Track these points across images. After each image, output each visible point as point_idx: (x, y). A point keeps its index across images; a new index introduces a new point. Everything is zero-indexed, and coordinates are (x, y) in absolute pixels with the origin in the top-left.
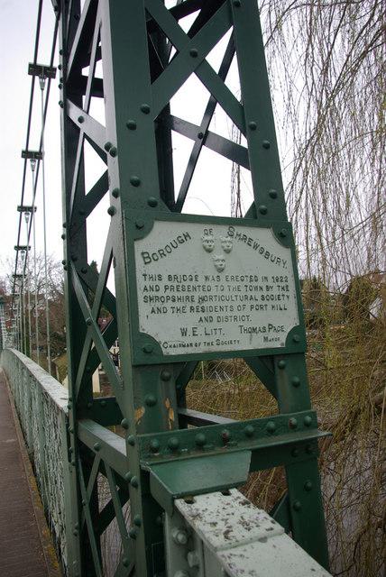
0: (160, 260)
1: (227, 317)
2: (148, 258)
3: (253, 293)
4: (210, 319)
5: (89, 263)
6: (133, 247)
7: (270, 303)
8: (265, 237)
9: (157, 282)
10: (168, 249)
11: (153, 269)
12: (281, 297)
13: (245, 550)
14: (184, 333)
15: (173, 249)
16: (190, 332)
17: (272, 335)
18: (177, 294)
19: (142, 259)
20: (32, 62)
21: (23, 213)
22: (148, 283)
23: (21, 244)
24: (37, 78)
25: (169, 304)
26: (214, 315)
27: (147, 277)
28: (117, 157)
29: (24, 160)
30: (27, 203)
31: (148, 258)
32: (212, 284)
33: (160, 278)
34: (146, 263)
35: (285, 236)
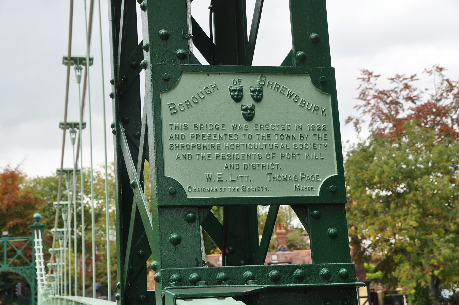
0: (174, 150)
1: (254, 165)
2: (174, 111)
3: (285, 143)
4: (236, 168)
5: (139, 42)
6: (160, 99)
7: (304, 153)
8: (303, 85)
9: (184, 132)
10: (194, 100)
11: (178, 120)
12: (318, 147)
13: (348, 142)
14: (209, 179)
15: (200, 100)
16: (215, 178)
17: (306, 185)
18: (203, 143)
19: (169, 110)
20: (66, 55)
21: (72, 68)
22: (174, 133)
23: (74, 54)
24: (72, 68)
25: (195, 152)
26: (242, 164)
27: (173, 127)
28: (149, 52)
29: (66, 67)
30: (79, 51)
31: (174, 111)
32: (240, 133)
33: (186, 127)
34: (172, 114)
35: (326, 82)
